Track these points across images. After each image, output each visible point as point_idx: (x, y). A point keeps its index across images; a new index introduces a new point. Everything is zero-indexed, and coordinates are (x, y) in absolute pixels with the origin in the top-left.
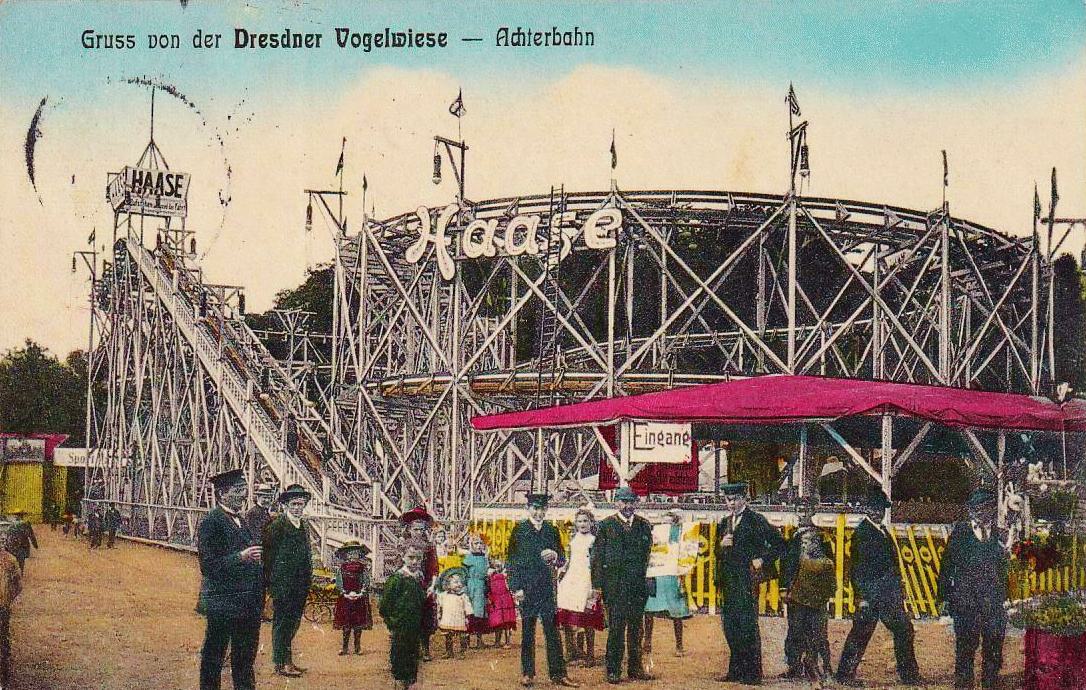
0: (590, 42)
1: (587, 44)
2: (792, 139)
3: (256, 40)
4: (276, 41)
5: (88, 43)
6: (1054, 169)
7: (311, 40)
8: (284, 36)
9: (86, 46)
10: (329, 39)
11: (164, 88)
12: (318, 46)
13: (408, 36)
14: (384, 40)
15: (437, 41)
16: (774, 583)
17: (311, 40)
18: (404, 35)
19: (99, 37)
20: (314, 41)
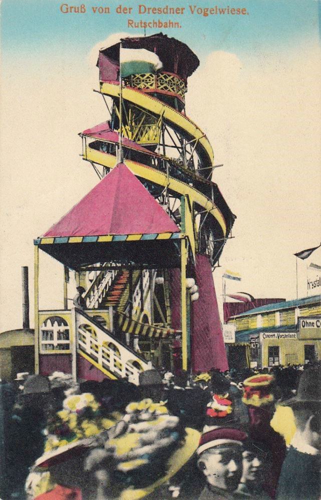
3: (151, 11)
14: (215, 12)
20: (128, 11)
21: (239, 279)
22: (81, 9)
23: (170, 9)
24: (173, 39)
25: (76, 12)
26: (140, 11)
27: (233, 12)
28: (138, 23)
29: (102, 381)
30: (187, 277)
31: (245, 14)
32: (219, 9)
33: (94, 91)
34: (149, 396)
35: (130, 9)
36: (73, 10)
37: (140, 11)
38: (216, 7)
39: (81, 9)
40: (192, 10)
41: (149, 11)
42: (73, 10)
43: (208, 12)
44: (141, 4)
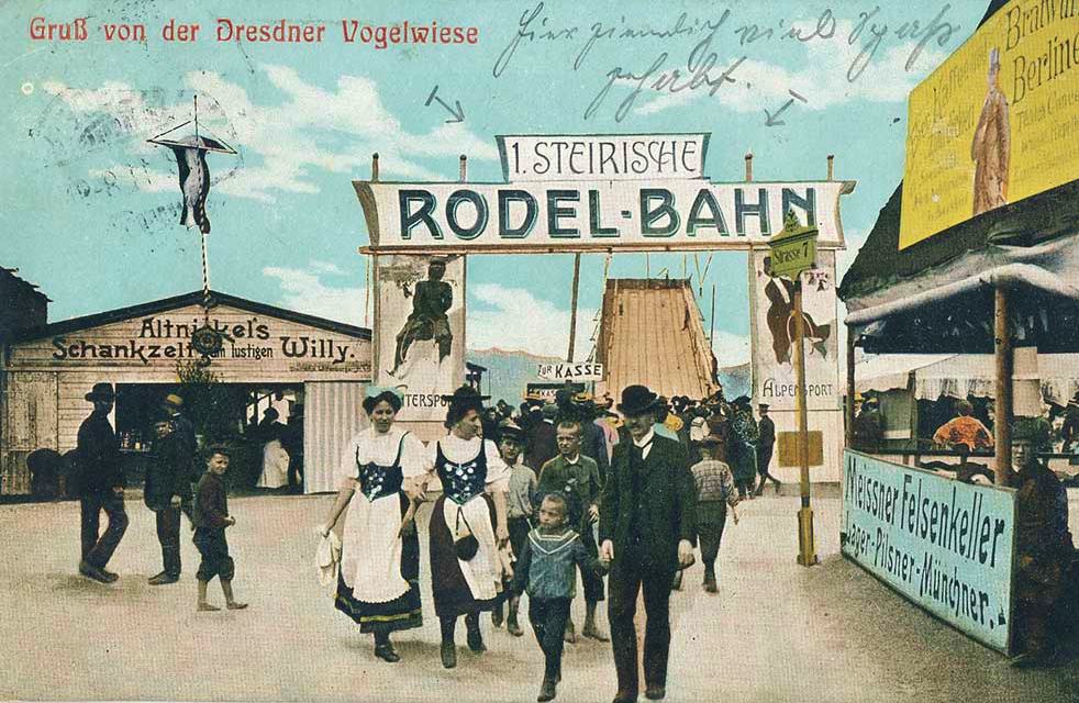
0: (65, 29)
1: (290, 40)
2: (85, 33)
3: (243, 34)
4: (267, 35)
5: (38, 34)
6: (437, 87)
7: (312, 34)
8: (277, 28)
9: (34, 37)
10: (207, 31)
11: (362, 140)
12: (193, 39)
13: (431, 31)
14: (402, 36)
15: (465, 37)
16: (284, 103)
17: (312, 34)
18: (427, 30)
19: (51, 28)
20: (189, 34)
21: (437, 87)
22: (76, 30)
23: (291, 28)
24: (437, 615)
25: (62, 38)
26: (143, 30)
27: (445, 38)
29: (681, 543)
30: (499, 191)
31: (448, 41)
32: (413, 29)
33: (376, 157)
34: (688, 476)
35: (194, 29)
36: (56, 32)
37: (143, 30)
38: (406, 23)
39: (76, 30)
40: (1000, 127)
41: (238, 32)
42: (56, 32)
44: (292, 25)
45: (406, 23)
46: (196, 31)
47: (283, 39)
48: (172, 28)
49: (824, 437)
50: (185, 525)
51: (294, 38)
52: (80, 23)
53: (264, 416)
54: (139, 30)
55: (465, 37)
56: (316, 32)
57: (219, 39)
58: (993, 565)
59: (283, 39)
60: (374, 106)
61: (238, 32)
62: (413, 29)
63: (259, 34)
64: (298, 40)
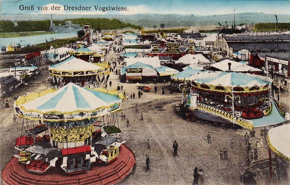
1: (83, 10)
3: (71, 8)
14: (109, 9)
23: (83, 7)
28: (30, 7)
32: (112, 8)
36: (27, 8)
41: (26, 8)
42: (27, 8)
43: (105, 9)
45: (110, 6)
46: (60, 8)
47: (80, 10)
48: (54, 7)
49: (159, 59)
50: (58, 82)
51: (46, 9)
52: (32, 6)
53: (42, 136)
54: (46, 8)
55: (124, 9)
56: (58, 8)
57: (65, 10)
58: (95, 6)
59: (80, 10)
60: (97, 89)
61: (26, 8)
62: (112, 8)
63: (121, 9)
64: (84, 10)
